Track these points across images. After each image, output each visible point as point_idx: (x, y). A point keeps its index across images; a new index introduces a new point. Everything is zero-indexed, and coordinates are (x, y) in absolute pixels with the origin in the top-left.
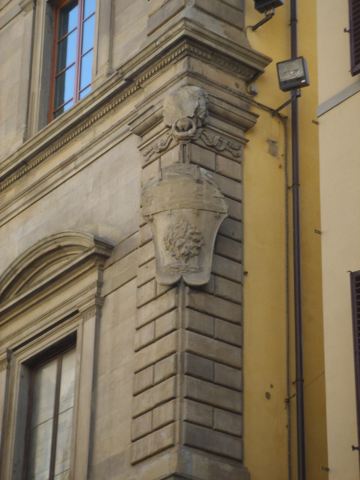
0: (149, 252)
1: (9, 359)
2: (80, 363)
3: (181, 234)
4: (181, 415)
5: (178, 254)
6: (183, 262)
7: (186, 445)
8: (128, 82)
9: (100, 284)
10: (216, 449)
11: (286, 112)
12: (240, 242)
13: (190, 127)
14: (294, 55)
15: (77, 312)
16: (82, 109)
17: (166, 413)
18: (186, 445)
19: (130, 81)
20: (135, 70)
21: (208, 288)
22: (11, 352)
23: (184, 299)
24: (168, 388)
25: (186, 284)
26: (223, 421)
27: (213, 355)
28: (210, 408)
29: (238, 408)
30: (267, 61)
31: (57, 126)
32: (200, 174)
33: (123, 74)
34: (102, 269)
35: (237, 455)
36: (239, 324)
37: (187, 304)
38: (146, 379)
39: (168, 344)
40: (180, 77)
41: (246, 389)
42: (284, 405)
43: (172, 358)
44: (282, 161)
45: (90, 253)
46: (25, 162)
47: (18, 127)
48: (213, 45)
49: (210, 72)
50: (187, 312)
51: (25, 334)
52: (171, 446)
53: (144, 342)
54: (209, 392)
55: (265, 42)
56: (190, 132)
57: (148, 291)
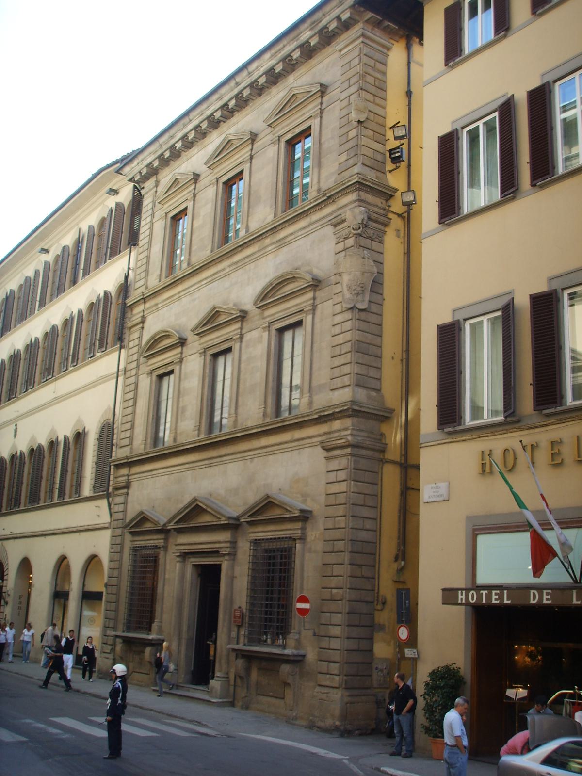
0: (338, 289)
1: (269, 327)
2: (305, 336)
3: (355, 284)
4: (354, 371)
5: (353, 293)
6: (355, 297)
7: (356, 385)
8: (328, 198)
9: (314, 298)
10: (369, 386)
11: (406, 215)
12: (382, 284)
13: (360, 228)
14: (409, 190)
15: (303, 310)
16: (304, 207)
17: (347, 369)
18: (356, 385)
19: (329, 197)
20: (332, 193)
21: (366, 313)
22: (270, 323)
23: (355, 315)
24: (348, 358)
25: (357, 308)
26: (373, 373)
27: (368, 342)
28: (367, 367)
29: (379, 366)
30: (396, 190)
31: (291, 213)
32: (364, 254)
33: (326, 194)
34: (315, 291)
35: (378, 388)
36: (381, 325)
37: (357, 318)
38: (337, 351)
39: (348, 336)
40: (355, 201)
41: (383, 356)
42: (400, 362)
43: (350, 343)
44: (402, 240)
45: (310, 284)
46: (275, 227)
47: (271, 207)
48: (371, 185)
49: (369, 197)
50: (357, 322)
51: (277, 315)
52: (349, 385)
53: (336, 333)
54: (367, 359)
55: (395, 180)
56: (359, 231)
57: (338, 308)
